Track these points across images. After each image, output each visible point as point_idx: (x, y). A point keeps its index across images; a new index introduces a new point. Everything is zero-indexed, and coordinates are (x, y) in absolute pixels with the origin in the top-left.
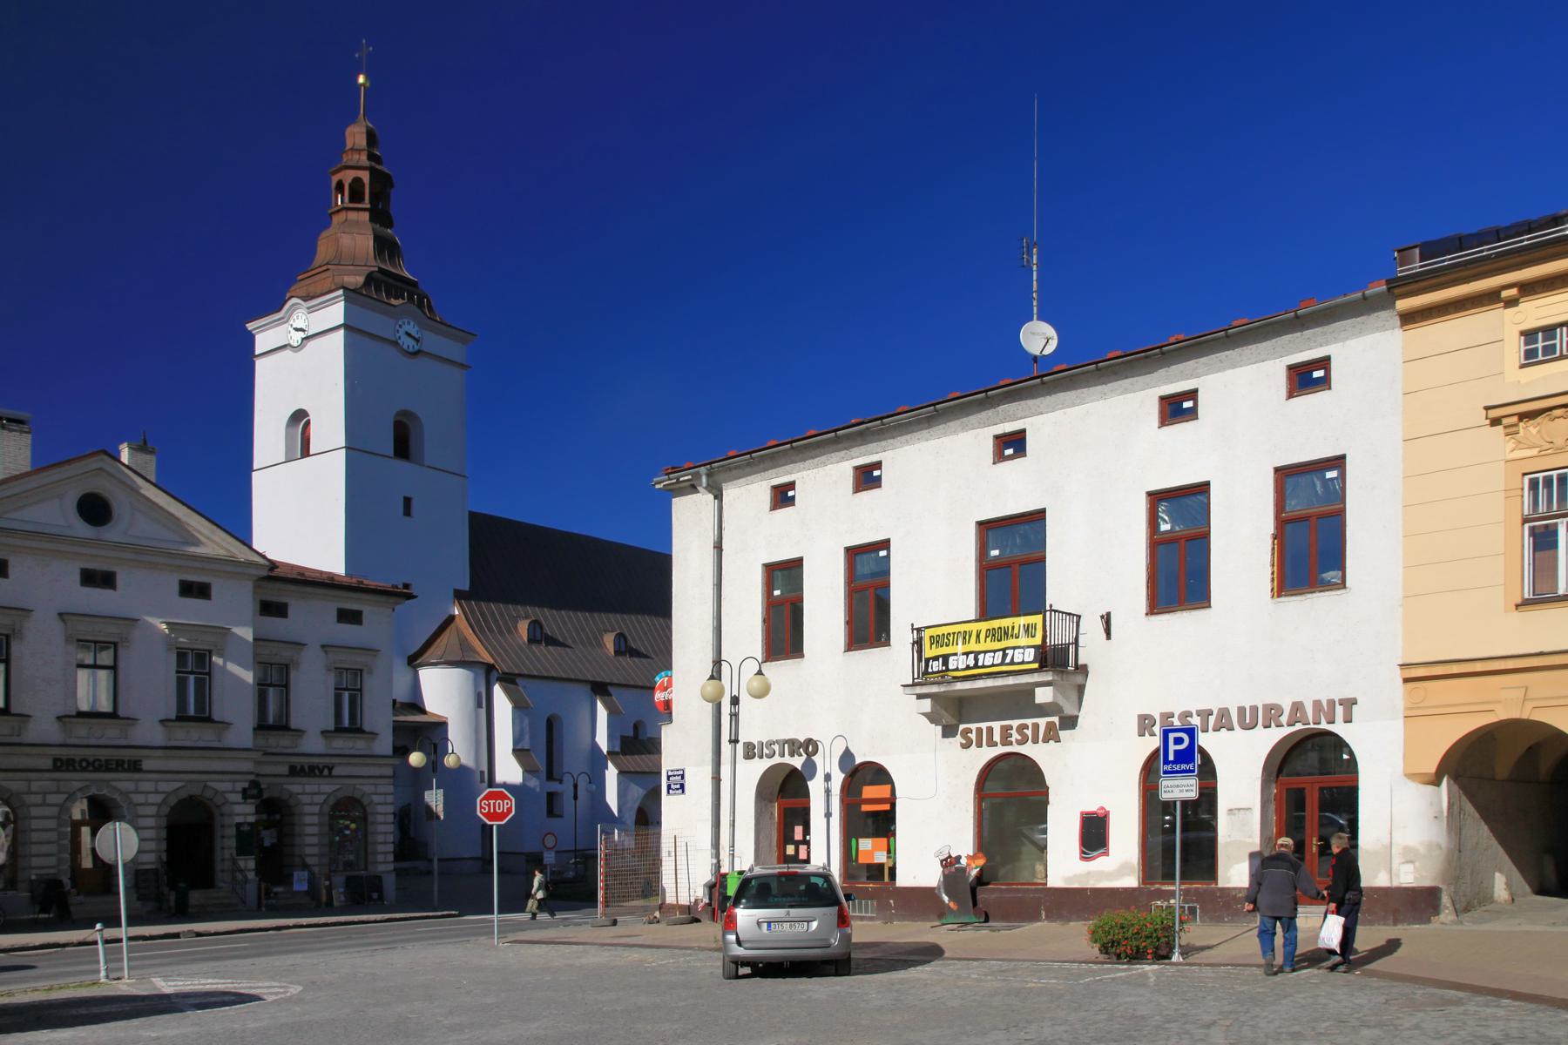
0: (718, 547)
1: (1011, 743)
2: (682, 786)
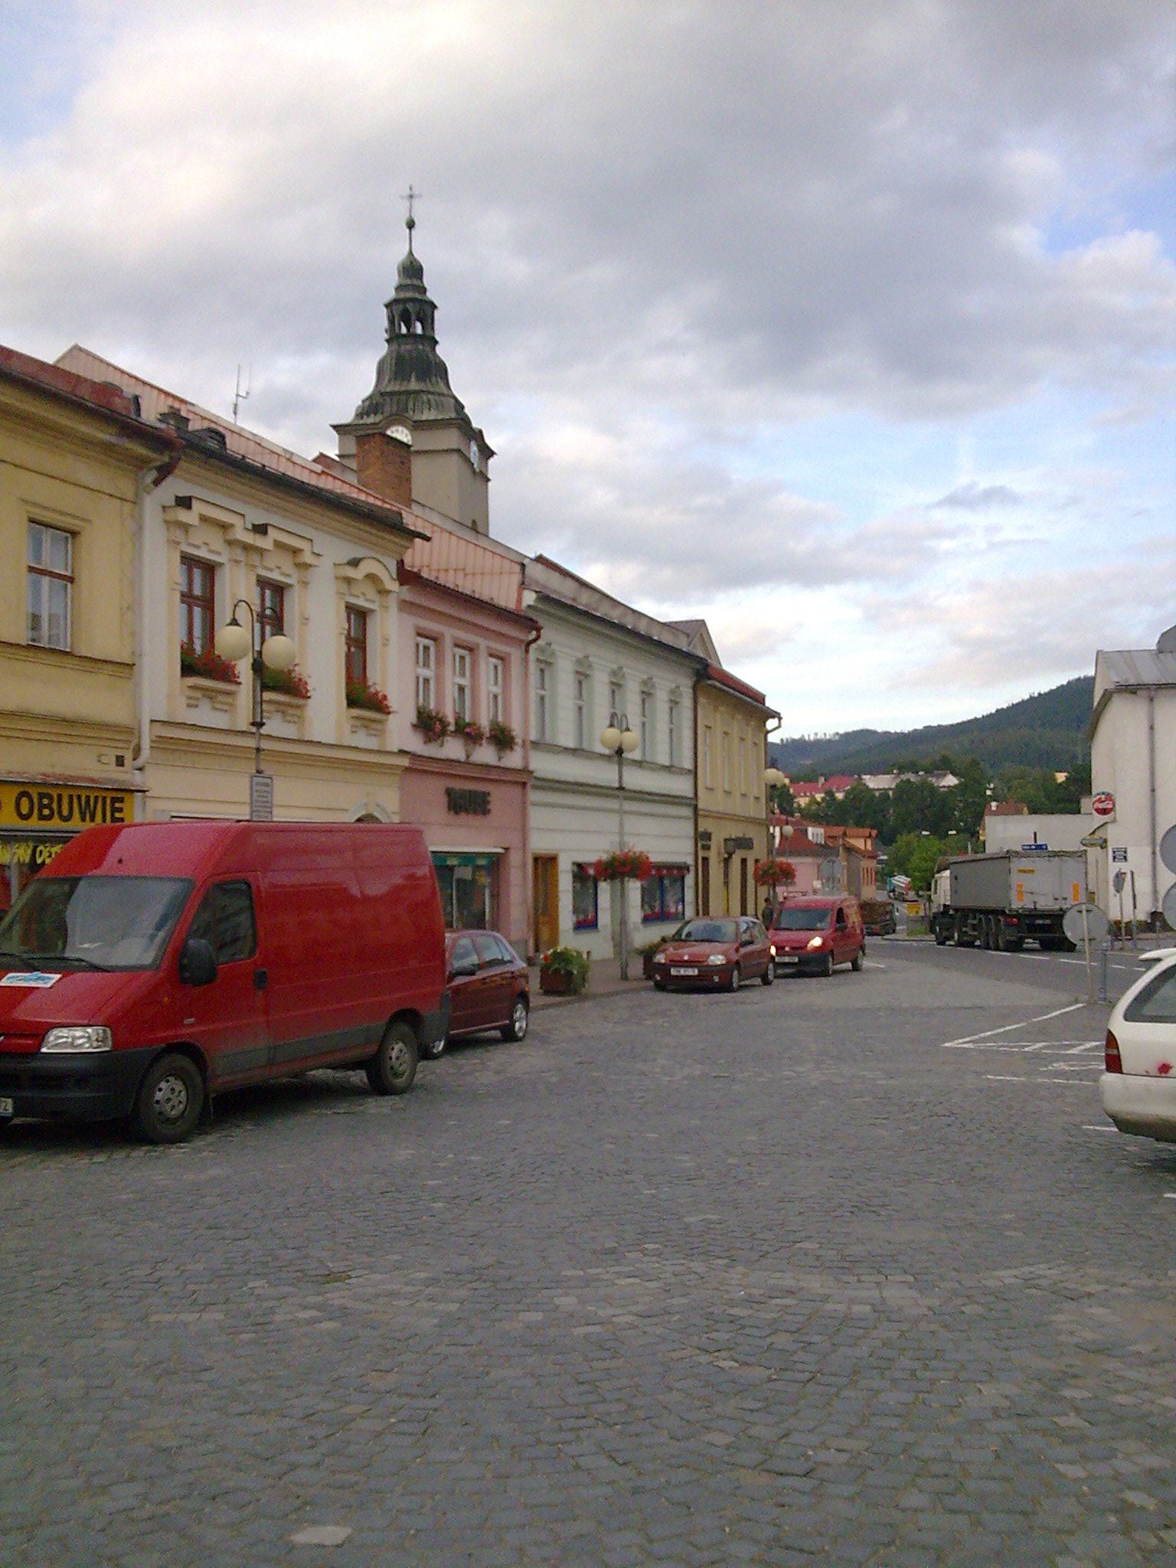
0: (1152, 728)
1: (746, 915)
2: (1125, 858)
